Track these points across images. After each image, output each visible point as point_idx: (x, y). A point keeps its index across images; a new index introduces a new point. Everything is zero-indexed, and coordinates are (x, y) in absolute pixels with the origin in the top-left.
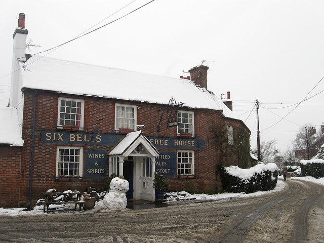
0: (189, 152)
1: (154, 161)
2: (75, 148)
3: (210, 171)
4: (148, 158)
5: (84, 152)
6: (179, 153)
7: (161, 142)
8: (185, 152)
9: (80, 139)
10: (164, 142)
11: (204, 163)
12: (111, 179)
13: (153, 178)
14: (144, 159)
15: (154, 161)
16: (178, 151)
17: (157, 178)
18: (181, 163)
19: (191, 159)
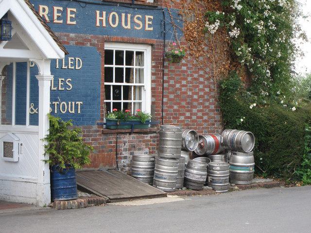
0: (134, 48)
1: (45, 71)
2: (134, 48)
3: (195, 111)
4: (22, 65)
5: (154, 58)
6: (109, 54)
7: (56, 14)
8: (125, 48)
9: (59, 18)
10: (64, 12)
11: (178, 86)
12: (213, 137)
13: (44, 128)
14: (7, 69)
15: (45, 71)
16: (108, 47)
17: (55, 131)
18: (114, 83)
19: (140, 72)
